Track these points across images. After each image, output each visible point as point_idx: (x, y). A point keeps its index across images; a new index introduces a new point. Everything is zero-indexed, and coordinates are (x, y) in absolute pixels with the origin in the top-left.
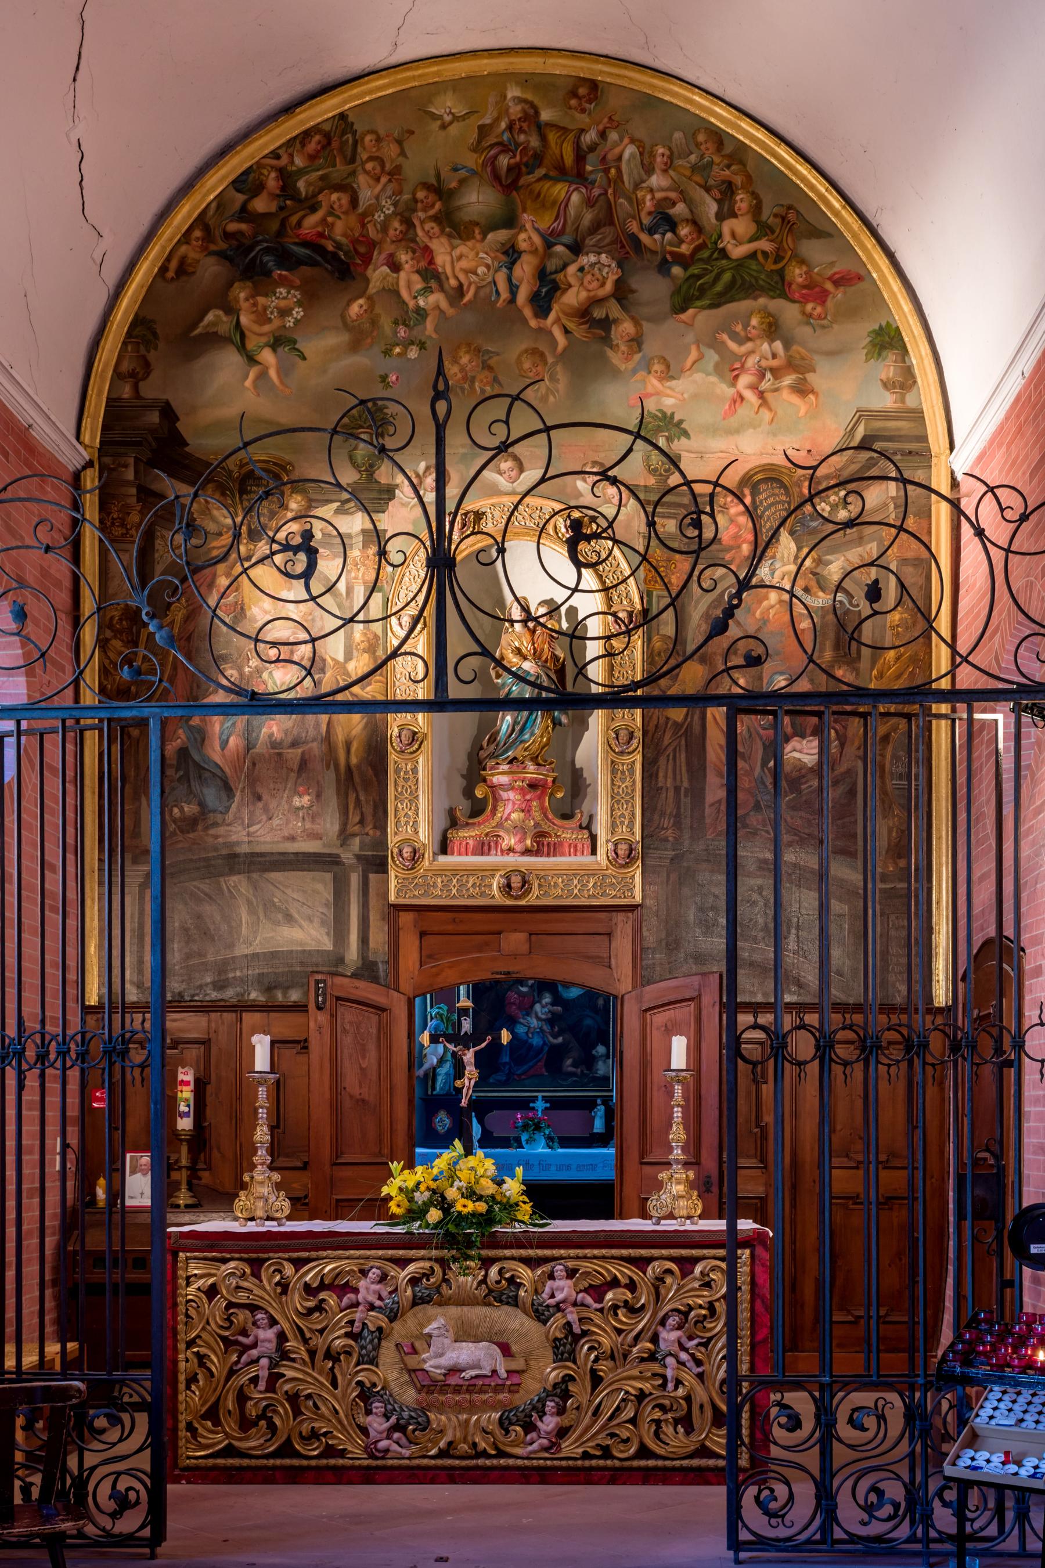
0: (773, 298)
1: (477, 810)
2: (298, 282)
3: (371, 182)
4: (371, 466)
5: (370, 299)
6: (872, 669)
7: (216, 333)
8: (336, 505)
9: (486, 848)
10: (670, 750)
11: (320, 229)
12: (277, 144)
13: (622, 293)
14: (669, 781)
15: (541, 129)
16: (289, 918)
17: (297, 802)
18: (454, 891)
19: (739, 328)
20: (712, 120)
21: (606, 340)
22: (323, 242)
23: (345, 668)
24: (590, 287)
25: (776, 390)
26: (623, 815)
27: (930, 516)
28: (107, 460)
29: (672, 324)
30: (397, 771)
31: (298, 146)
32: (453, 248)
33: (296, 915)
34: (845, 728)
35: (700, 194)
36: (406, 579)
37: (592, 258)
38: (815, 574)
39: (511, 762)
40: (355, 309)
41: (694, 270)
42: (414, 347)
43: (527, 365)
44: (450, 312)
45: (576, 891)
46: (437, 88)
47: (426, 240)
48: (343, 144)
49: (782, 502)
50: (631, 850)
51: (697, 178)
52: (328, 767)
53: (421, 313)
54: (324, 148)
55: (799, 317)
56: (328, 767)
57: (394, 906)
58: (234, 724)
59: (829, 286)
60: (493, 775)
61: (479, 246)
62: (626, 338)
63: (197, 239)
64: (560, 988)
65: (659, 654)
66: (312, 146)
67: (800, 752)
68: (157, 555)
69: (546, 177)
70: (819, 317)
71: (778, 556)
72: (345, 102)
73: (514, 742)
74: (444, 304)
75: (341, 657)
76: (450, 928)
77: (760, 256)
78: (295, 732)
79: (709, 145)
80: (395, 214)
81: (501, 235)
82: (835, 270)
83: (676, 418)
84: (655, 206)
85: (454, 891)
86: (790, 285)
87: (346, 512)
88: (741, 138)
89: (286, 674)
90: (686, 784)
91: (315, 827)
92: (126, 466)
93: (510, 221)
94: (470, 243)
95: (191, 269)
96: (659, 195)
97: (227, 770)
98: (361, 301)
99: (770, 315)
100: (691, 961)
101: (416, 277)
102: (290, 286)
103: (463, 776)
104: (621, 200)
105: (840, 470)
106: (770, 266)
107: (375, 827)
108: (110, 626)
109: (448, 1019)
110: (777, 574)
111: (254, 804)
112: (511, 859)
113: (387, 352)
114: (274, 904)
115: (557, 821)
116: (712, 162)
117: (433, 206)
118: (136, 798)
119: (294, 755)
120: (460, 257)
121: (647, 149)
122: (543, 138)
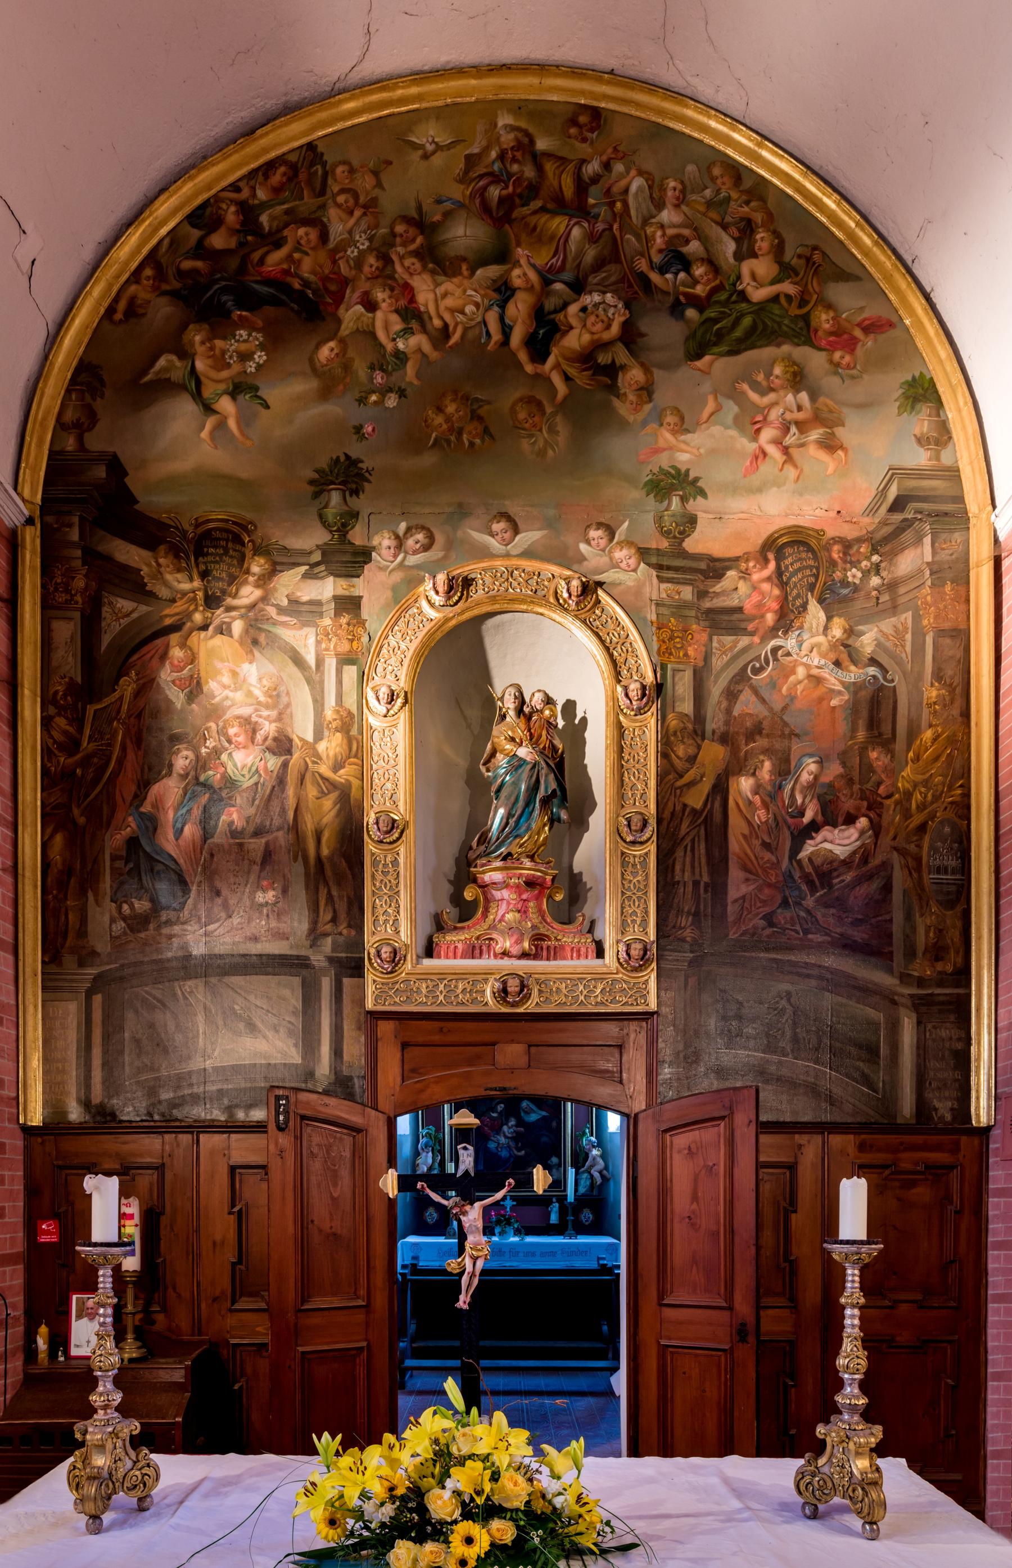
0: (799, 345)
1: (466, 911)
2: (260, 323)
3: (343, 215)
4: (344, 525)
5: (342, 342)
6: (908, 751)
7: (168, 380)
8: (304, 569)
9: (477, 951)
10: (688, 841)
11: (285, 266)
12: (239, 174)
13: (630, 336)
14: (686, 874)
15: (537, 159)
16: (252, 1028)
17: (260, 897)
18: (441, 998)
19: (761, 377)
20: (730, 152)
21: (612, 388)
22: (289, 279)
23: (315, 750)
24: (594, 329)
25: (802, 445)
26: (634, 913)
27: (968, 583)
28: (50, 519)
29: (686, 372)
30: (375, 863)
31: (261, 178)
32: (437, 285)
33: (259, 1024)
34: (880, 816)
35: (715, 231)
36: (384, 651)
37: (597, 298)
38: (846, 646)
39: (504, 859)
40: (326, 352)
41: (711, 313)
42: (393, 395)
43: (522, 415)
44: (434, 355)
45: (582, 998)
46: (416, 117)
47: (406, 276)
48: (312, 176)
49: (811, 567)
50: (645, 950)
51: (713, 215)
52: (295, 859)
53: (401, 357)
54: (290, 180)
55: (827, 366)
56: (295, 859)
57: (371, 1013)
58: (189, 811)
59: (858, 333)
60: (484, 872)
61: (466, 282)
62: (635, 387)
63: (148, 278)
64: (522, 1114)
65: (675, 734)
66: (277, 177)
67: (831, 842)
68: (103, 624)
69: (543, 209)
70: (848, 367)
71: (806, 626)
72: (314, 129)
73: (507, 837)
74: (427, 347)
75: (310, 737)
76: (436, 1038)
77: (783, 300)
78: (258, 820)
79: (725, 179)
80: (370, 249)
81: (493, 271)
82: (865, 315)
83: (692, 475)
84: (667, 243)
85: (441, 998)
86: (816, 331)
87: (316, 577)
88: (762, 172)
89: (248, 755)
90: (706, 878)
91: (282, 925)
92: (70, 525)
93: (502, 256)
94: (455, 280)
95: (141, 311)
96: (670, 232)
97: (181, 861)
98: (332, 344)
99: (794, 363)
100: (712, 1076)
101: (394, 318)
102: (252, 328)
103: (450, 881)
104: (628, 236)
105: (872, 532)
106: (794, 311)
107: (349, 926)
108: (54, 702)
109: (435, 1137)
110: (806, 646)
111: (212, 899)
112: (506, 962)
113: (362, 401)
114: (235, 1013)
115: (556, 925)
116: (729, 199)
117: (413, 240)
118: (82, 893)
119: (257, 845)
120: (445, 295)
121: (657, 180)
122: (540, 169)
